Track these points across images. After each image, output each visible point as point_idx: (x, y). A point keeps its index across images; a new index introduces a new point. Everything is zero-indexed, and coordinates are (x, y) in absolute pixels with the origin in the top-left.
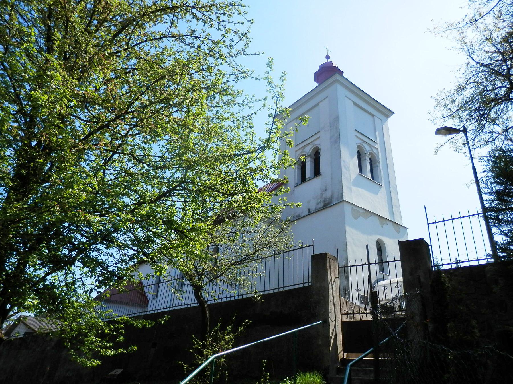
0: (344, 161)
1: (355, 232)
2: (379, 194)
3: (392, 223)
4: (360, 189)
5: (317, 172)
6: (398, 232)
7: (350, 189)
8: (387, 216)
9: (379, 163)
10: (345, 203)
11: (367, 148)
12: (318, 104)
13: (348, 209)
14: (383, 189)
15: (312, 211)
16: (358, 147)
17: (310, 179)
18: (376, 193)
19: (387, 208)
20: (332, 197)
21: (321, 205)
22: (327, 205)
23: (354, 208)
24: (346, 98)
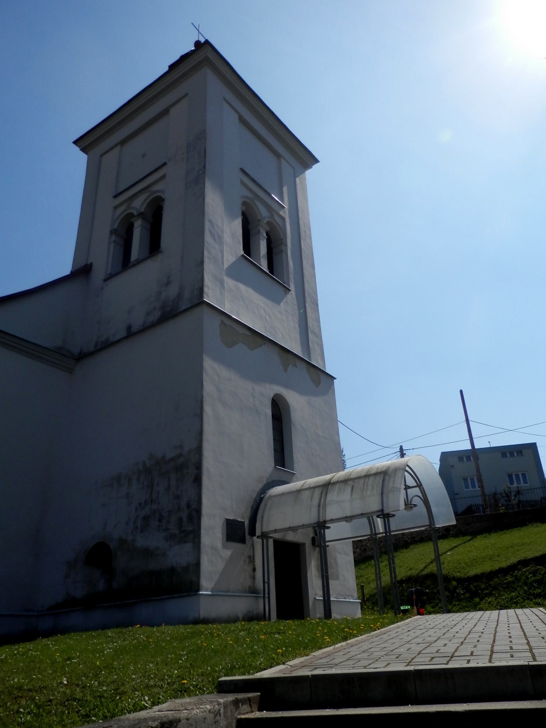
0: (210, 221)
1: (225, 373)
2: (282, 304)
3: (304, 365)
4: (242, 287)
5: (154, 246)
6: (317, 383)
7: (222, 283)
8: (297, 350)
9: (286, 245)
10: (205, 309)
11: (264, 212)
12: (165, 112)
13: (211, 324)
14: (292, 296)
15: (134, 329)
16: (244, 204)
17: (139, 262)
18: (277, 301)
19: (296, 335)
20: (179, 296)
21: (156, 315)
22: (169, 313)
23: (227, 322)
24: (225, 105)
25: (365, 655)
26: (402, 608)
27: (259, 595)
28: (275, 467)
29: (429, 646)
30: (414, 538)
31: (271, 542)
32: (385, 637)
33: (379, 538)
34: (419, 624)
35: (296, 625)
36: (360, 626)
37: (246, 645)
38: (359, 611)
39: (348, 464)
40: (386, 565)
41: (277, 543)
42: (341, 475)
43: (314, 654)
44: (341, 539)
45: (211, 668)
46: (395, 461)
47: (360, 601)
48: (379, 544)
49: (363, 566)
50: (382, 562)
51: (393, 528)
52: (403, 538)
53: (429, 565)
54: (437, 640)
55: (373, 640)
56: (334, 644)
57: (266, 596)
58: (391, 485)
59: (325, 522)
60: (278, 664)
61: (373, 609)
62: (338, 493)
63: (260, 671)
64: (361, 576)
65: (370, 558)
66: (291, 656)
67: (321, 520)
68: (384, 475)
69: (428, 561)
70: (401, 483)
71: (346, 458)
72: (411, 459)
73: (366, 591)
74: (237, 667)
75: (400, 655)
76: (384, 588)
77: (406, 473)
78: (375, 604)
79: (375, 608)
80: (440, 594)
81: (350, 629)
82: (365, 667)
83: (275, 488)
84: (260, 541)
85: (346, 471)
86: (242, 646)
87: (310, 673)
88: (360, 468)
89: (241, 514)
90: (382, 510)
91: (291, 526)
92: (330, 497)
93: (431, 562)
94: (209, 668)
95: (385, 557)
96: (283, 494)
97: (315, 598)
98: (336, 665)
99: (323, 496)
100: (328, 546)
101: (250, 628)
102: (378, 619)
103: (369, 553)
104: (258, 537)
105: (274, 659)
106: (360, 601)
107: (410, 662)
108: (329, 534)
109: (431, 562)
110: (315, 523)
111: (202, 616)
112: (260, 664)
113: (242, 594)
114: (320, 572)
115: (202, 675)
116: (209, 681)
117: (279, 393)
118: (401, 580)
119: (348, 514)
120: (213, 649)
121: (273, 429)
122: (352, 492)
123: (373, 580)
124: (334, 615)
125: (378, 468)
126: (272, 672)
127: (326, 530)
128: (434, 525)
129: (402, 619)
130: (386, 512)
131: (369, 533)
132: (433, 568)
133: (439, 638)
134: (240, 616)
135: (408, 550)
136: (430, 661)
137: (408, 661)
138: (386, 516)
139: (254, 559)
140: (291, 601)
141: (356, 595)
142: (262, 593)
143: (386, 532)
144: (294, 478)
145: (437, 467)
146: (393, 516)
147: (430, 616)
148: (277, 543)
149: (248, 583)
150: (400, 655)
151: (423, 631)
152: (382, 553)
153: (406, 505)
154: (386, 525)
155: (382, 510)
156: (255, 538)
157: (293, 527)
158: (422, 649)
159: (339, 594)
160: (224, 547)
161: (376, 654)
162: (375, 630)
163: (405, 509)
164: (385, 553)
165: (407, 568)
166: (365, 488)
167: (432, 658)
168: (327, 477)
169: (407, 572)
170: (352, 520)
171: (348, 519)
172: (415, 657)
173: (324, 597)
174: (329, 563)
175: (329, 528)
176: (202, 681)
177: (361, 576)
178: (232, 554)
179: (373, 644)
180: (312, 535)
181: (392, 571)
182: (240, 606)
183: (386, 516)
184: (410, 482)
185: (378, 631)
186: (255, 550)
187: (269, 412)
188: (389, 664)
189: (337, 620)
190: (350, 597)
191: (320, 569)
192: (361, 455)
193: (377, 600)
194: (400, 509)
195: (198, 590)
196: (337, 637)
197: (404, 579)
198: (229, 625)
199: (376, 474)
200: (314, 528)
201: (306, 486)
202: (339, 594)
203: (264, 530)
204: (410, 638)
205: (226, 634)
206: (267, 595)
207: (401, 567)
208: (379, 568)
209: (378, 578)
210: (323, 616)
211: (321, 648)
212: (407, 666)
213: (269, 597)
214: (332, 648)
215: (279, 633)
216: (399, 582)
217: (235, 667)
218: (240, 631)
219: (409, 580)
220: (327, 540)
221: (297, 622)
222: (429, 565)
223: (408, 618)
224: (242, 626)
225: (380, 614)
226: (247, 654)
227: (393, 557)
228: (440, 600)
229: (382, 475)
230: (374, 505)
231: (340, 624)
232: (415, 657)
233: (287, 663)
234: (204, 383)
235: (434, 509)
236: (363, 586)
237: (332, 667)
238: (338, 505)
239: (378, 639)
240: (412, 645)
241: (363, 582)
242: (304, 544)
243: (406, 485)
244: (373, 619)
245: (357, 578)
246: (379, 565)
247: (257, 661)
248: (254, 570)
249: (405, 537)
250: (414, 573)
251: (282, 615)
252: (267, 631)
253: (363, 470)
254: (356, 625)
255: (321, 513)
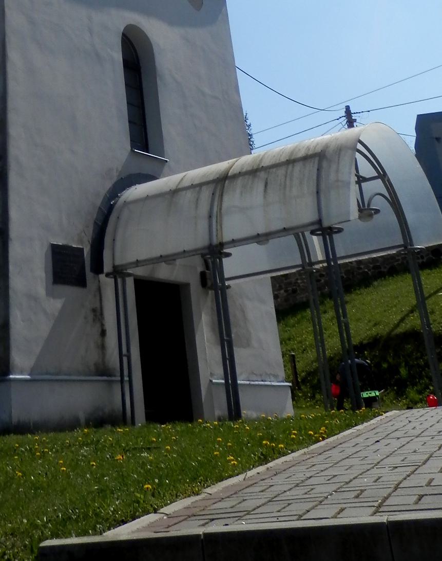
25: (299, 492)
26: (365, 395)
27: (113, 378)
28: (132, 151)
29: (413, 472)
30: (379, 267)
31: (130, 282)
32: (335, 454)
33: (318, 270)
34: (394, 428)
35: (177, 431)
36: (290, 434)
37: (91, 474)
38: (290, 402)
39: (257, 140)
40: (333, 318)
41: (142, 285)
42: (245, 161)
43: (208, 490)
44: (251, 275)
45: (28, 520)
46: (339, 133)
47: (290, 384)
48: (318, 281)
49: (292, 321)
50: (325, 312)
51: (340, 252)
52: (359, 268)
53: (407, 315)
54: (428, 459)
55: (315, 460)
56: (245, 469)
57: (125, 381)
58: (332, 177)
59: (222, 245)
60: (146, 512)
61: (313, 397)
62: (241, 193)
63: (115, 527)
64: (289, 339)
65: (304, 306)
66: (168, 496)
67: (215, 241)
68: (319, 159)
69: (406, 309)
70: (350, 173)
71: (253, 130)
72: (365, 130)
73: (299, 366)
74: (74, 517)
75: (362, 491)
76: (331, 359)
77: (358, 155)
78: (316, 388)
79: (318, 396)
80: (429, 368)
81: (272, 439)
82: (300, 518)
83: (133, 188)
84: (111, 281)
85: (256, 153)
86: (83, 477)
87: (200, 531)
88: (278, 149)
89: (76, 236)
90: (320, 222)
91: (164, 253)
92: (228, 201)
93: (412, 311)
94: (25, 521)
95: (329, 303)
96: (148, 198)
97: (211, 381)
98: (249, 513)
99: (216, 203)
100: (229, 287)
101: (98, 441)
102: (322, 418)
103: (302, 297)
104: (108, 275)
105: (138, 502)
106: (290, 384)
107: (380, 506)
108: (230, 266)
109: (412, 311)
110: (204, 248)
111: (15, 420)
112: (115, 511)
113: (83, 378)
114: (218, 335)
115: (12, 534)
116: (25, 546)
117: (132, 23)
118: (361, 343)
119: (261, 230)
120: (32, 482)
121: (126, 85)
122: (265, 191)
123: (311, 345)
124: (244, 412)
125: (308, 148)
126: (135, 528)
127: (224, 260)
128: (412, 244)
129: (365, 419)
130: (326, 224)
131: (299, 262)
132: (414, 321)
133: (431, 456)
134: (82, 417)
135: (371, 289)
136: (416, 503)
137: (376, 504)
138: (327, 232)
139: (102, 314)
140: (170, 391)
141: (282, 374)
142: (119, 374)
143: (328, 260)
144: (166, 169)
145: (411, 140)
146: (340, 230)
147: (414, 411)
148: (142, 285)
149: (93, 357)
150: (362, 491)
151: (403, 441)
152: (324, 296)
153: (360, 210)
154: (329, 248)
155: (320, 222)
156: (102, 277)
157: (167, 256)
158: (401, 478)
159: (253, 373)
160: (50, 294)
161: (319, 489)
162: (317, 441)
163: (360, 218)
164: (330, 296)
165: (369, 321)
166: (288, 183)
167: (421, 497)
168: (222, 166)
169: (370, 329)
170: (268, 240)
171: (261, 238)
172: (389, 495)
173: (226, 379)
174: (231, 318)
175: (228, 255)
176: (13, 546)
177: (289, 339)
178: (64, 307)
179: (314, 468)
180: (200, 269)
181: (344, 328)
182: (80, 398)
183: (327, 232)
184: (366, 170)
185: (322, 443)
186: (103, 299)
187: (118, 56)
188: (342, 510)
189: (251, 421)
190: (272, 378)
191: (217, 330)
192: (279, 125)
193: (319, 381)
194: (352, 218)
195: (7, 371)
196: (249, 456)
197: (365, 342)
198: (61, 435)
199: (306, 158)
200: (203, 256)
201: (186, 183)
202: (253, 373)
203: (117, 263)
204: (379, 457)
205: (57, 451)
206: (126, 378)
207: (358, 320)
208: (320, 323)
209: (320, 342)
210: (226, 413)
211: (221, 479)
212: (374, 513)
213: (130, 382)
214: (241, 477)
215: (149, 449)
216: (356, 348)
217: (70, 518)
218: (81, 447)
219: (374, 343)
220: (226, 276)
221: (180, 427)
222: (407, 315)
223: (375, 417)
224: (86, 435)
225: (326, 409)
226: (92, 492)
227: (344, 303)
228: (430, 379)
229: (317, 159)
230: (305, 214)
231: (257, 429)
232: (389, 495)
233: (162, 510)
234: (6, 10)
235: (410, 217)
236: (293, 356)
237: (240, 518)
238: (243, 215)
239: (322, 457)
240: (382, 471)
241: (293, 350)
242: (187, 285)
243: (358, 176)
244: (315, 419)
245: (283, 342)
246: (319, 318)
247: (109, 506)
248: (103, 333)
249: (362, 267)
250: (382, 330)
251: (155, 415)
252: (127, 445)
253: (282, 151)
254: (284, 432)
255: (214, 230)
